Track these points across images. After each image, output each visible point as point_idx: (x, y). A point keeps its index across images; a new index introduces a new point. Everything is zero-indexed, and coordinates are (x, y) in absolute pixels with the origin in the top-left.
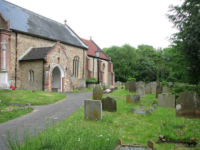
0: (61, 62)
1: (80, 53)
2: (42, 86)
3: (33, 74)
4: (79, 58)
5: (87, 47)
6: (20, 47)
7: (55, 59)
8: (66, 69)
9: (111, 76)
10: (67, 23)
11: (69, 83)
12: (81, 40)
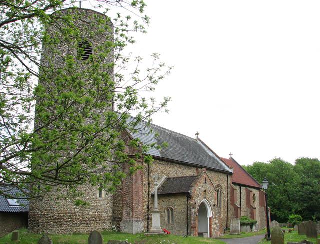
0: (209, 195)
1: (222, 180)
2: (186, 229)
3: (173, 214)
4: (222, 188)
5: (231, 171)
6: (154, 176)
8: (214, 205)
10: (200, 137)
11: (219, 224)
12: (222, 160)
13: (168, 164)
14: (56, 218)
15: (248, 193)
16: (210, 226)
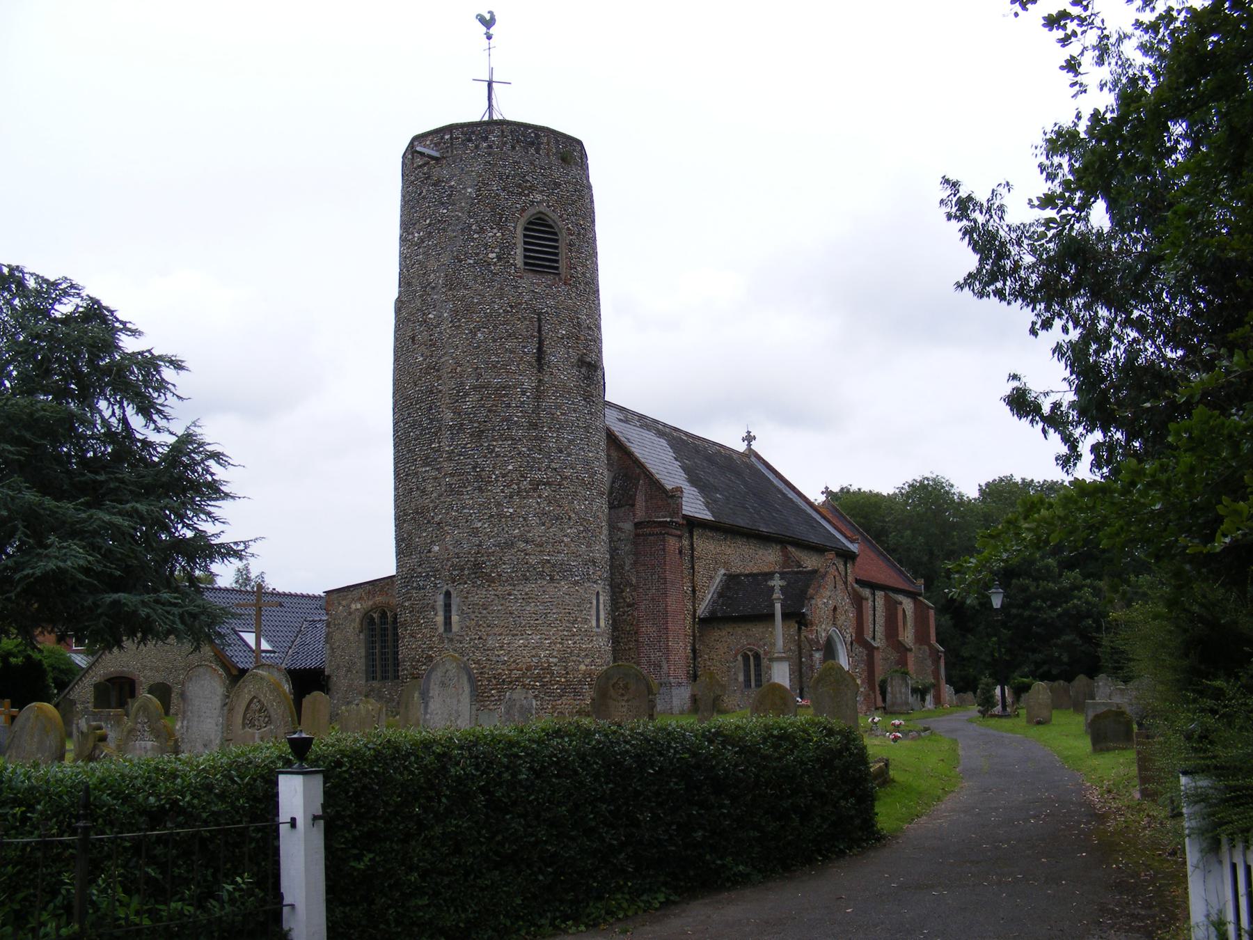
0: (841, 619)
5: (854, 548)
8: (852, 643)
9: (929, 662)
10: (755, 446)
13: (725, 539)
14: (504, 681)
15: (892, 607)
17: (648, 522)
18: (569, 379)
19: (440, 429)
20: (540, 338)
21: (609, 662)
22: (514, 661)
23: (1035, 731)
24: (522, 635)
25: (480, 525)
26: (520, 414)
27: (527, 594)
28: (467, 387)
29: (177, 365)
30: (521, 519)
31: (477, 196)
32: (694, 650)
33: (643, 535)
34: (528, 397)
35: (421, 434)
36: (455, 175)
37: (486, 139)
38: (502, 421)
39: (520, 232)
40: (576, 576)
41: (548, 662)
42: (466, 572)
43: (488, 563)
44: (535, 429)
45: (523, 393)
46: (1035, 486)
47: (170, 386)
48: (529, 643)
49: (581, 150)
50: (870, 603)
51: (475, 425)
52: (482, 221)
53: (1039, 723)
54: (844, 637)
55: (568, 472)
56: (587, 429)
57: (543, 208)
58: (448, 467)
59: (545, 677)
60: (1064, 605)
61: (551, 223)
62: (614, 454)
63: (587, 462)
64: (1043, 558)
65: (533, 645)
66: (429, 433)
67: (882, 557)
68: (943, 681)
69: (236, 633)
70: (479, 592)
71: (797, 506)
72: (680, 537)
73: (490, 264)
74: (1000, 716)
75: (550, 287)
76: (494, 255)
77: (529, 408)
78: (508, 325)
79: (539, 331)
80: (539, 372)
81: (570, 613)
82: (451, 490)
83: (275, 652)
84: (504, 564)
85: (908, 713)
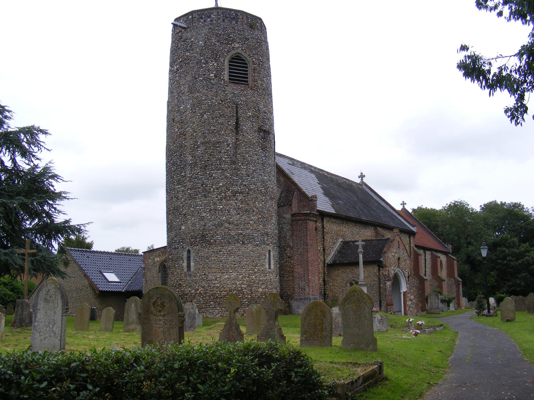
0: (402, 264)
5: (414, 229)
7: (395, 259)
8: (409, 277)
9: (454, 286)
10: (365, 180)
11: (414, 301)
13: (342, 223)
14: (217, 297)
15: (434, 260)
16: (405, 303)
17: (298, 214)
18: (253, 138)
19: (186, 166)
20: (237, 117)
21: (276, 287)
22: (223, 287)
23: (505, 326)
24: (227, 273)
25: (205, 214)
26: (226, 157)
27: (229, 251)
28: (199, 143)
29: (44, 132)
30: (226, 212)
31: (205, 45)
32: (324, 281)
33: (296, 220)
34: (231, 148)
35: (177, 168)
36: (194, 36)
37: (209, 17)
38: (217, 160)
39: (227, 63)
40: (257, 241)
41: (241, 287)
42: (198, 240)
43: (209, 235)
44: (234, 164)
45: (228, 145)
46: (507, 205)
47: (41, 143)
48: (230, 277)
49: (261, 23)
50: (423, 257)
51: (203, 163)
52: (207, 58)
53: (508, 321)
54: (404, 274)
55: (252, 187)
56: (263, 164)
57: (239, 50)
58: (189, 185)
59: (240, 295)
60: (522, 260)
61: (244, 58)
62: (282, 179)
63: (263, 182)
64: (511, 238)
65: (233, 278)
66: (180, 168)
67: (431, 235)
68: (461, 296)
69: (101, 273)
70: (204, 250)
71: (386, 209)
72: (316, 221)
73: (211, 80)
74: (487, 316)
75: (243, 91)
76: (213, 75)
77: (231, 153)
78: (220, 110)
79: (237, 113)
80: (237, 134)
81: (253, 261)
82: (191, 197)
83: (121, 282)
84: (218, 235)
85: (439, 313)
